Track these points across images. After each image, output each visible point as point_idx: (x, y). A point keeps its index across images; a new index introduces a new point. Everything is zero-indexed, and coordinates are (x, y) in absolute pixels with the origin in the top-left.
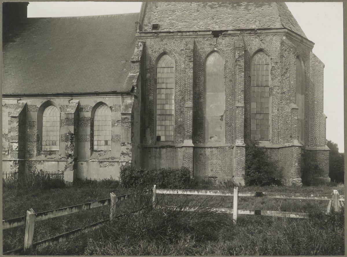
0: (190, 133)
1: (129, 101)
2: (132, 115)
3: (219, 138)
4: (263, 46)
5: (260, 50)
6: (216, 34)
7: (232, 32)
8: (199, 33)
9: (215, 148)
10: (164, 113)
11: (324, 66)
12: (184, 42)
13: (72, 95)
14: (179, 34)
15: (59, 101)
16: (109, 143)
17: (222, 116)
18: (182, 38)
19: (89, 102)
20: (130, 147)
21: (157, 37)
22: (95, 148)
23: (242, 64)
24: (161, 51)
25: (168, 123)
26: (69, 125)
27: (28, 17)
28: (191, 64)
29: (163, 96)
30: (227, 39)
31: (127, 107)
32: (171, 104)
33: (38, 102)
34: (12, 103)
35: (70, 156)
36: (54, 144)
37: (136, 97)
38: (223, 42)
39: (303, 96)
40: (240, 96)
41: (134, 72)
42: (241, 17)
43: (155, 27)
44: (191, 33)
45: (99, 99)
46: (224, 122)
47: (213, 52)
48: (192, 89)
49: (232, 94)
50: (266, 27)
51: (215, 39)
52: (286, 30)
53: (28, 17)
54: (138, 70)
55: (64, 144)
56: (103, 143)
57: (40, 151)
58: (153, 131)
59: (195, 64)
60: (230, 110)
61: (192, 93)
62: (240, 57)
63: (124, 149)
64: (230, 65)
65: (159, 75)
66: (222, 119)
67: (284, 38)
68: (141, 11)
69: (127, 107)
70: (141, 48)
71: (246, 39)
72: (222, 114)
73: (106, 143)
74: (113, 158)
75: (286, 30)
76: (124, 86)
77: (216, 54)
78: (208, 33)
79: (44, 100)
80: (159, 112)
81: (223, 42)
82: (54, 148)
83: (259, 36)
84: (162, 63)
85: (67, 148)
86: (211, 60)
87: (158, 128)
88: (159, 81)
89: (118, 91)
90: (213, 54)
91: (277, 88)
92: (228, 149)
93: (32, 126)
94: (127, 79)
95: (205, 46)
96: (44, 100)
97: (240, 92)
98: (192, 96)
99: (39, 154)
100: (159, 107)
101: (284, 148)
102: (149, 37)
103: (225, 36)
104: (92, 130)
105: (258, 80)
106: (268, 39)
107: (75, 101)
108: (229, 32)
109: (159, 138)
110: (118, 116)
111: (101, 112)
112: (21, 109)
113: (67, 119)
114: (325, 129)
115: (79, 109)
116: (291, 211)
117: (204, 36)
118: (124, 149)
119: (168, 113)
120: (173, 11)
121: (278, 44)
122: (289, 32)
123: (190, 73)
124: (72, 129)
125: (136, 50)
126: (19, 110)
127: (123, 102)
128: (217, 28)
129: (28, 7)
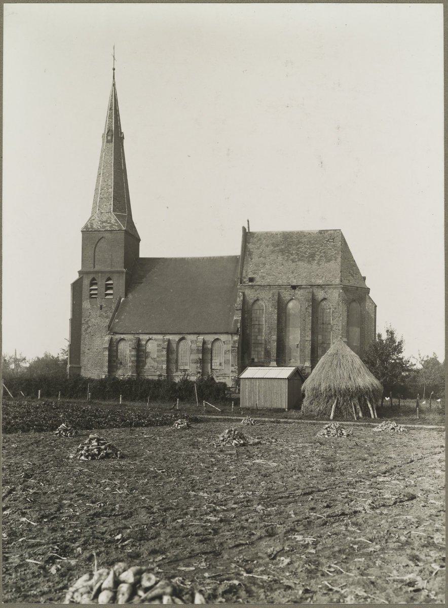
0: (275, 358)
1: (236, 338)
2: (238, 348)
3: (296, 360)
4: (326, 296)
5: (325, 299)
6: (294, 287)
7: (304, 287)
8: (282, 287)
10: (248, 404)
12: (271, 292)
13: (199, 334)
14: (268, 287)
15: (190, 338)
16: (223, 364)
17: (298, 345)
18: (270, 290)
19: (210, 338)
20: (237, 367)
21: (252, 288)
22: (213, 367)
23: (311, 311)
24: (255, 298)
25: (260, 349)
26: (199, 353)
27: (141, 256)
28: (276, 311)
29: (256, 330)
30: (302, 291)
31: (235, 342)
32: (262, 336)
33: (176, 338)
35: (199, 372)
36: (186, 365)
37: (239, 335)
38: (299, 292)
39: (359, 329)
41: (237, 317)
42: (313, 272)
43: (251, 280)
44: (276, 287)
45: (216, 336)
46: (299, 349)
47: (292, 299)
48: (276, 327)
49: (303, 330)
51: (293, 291)
52: (342, 286)
53: (141, 256)
54: (240, 315)
55: (194, 366)
56: (218, 364)
57: (177, 369)
58: (250, 354)
59: (278, 309)
60: (303, 341)
61: (276, 330)
62: (309, 306)
63: (233, 368)
64: (303, 309)
65: (253, 315)
66: (297, 347)
67: (341, 291)
68: (242, 253)
69: (235, 342)
70: (242, 298)
71: (315, 291)
73: (220, 364)
74: (225, 374)
76: (232, 328)
78: (288, 287)
79: (181, 336)
80: (253, 341)
81: (299, 293)
82: (186, 368)
83: (324, 289)
84: (256, 307)
85: (197, 367)
86: (291, 305)
87: (253, 353)
88: (255, 319)
89: (229, 332)
90: (292, 301)
93: (172, 353)
95: (286, 295)
96: (181, 336)
98: (276, 332)
99: (177, 371)
100: (253, 338)
103: (300, 288)
104: (212, 356)
105: (323, 320)
106: (330, 291)
107: (201, 338)
108: (303, 286)
109: (253, 359)
110: (229, 347)
111: (217, 344)
113: (198, 350)
115: (204, 343)
117: (285, 289)
118: (233, 368)
119: (260, 342)
120: (264, 264)
121: (337, 295)
123: (275, 317)
124: (200, 356)
125: (238, 299)
127: (232, 339)
128: (294, 284)
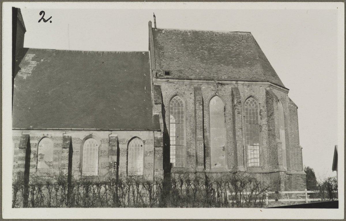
4: (253, 94)
9: (262, 173)
11: (297, 108)
26: (113, 155)
34: (57, 136)
40: (239, 133)
50: (254, 79)
72: (224, 146)
75: (269, 83)
77: (217, 96)
91: (265, 125)
92: (158, 173)
94: (153, 118)
97: (239, 129)
101: (273, 173)
102: (163, 81)
112: (69, 141)
114: (302, 157)
116: (274, 129)
122: (271, 84)
126: (67, 142)
129: (25, 34)
